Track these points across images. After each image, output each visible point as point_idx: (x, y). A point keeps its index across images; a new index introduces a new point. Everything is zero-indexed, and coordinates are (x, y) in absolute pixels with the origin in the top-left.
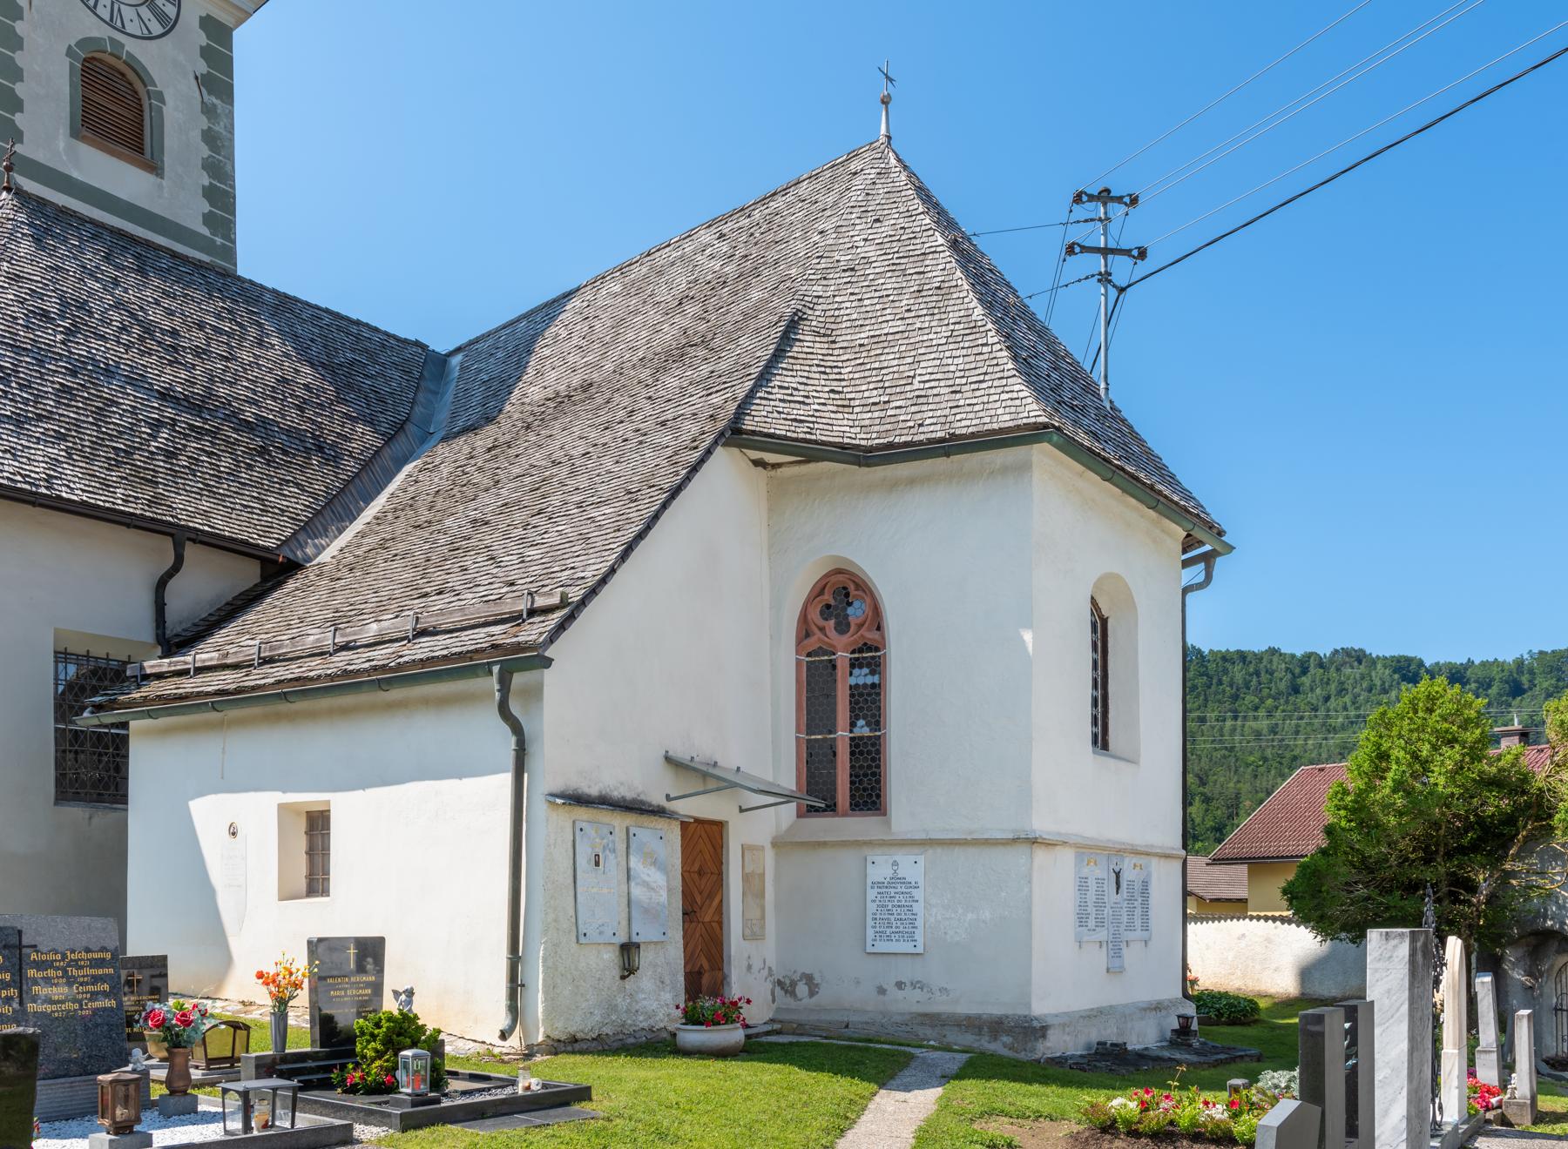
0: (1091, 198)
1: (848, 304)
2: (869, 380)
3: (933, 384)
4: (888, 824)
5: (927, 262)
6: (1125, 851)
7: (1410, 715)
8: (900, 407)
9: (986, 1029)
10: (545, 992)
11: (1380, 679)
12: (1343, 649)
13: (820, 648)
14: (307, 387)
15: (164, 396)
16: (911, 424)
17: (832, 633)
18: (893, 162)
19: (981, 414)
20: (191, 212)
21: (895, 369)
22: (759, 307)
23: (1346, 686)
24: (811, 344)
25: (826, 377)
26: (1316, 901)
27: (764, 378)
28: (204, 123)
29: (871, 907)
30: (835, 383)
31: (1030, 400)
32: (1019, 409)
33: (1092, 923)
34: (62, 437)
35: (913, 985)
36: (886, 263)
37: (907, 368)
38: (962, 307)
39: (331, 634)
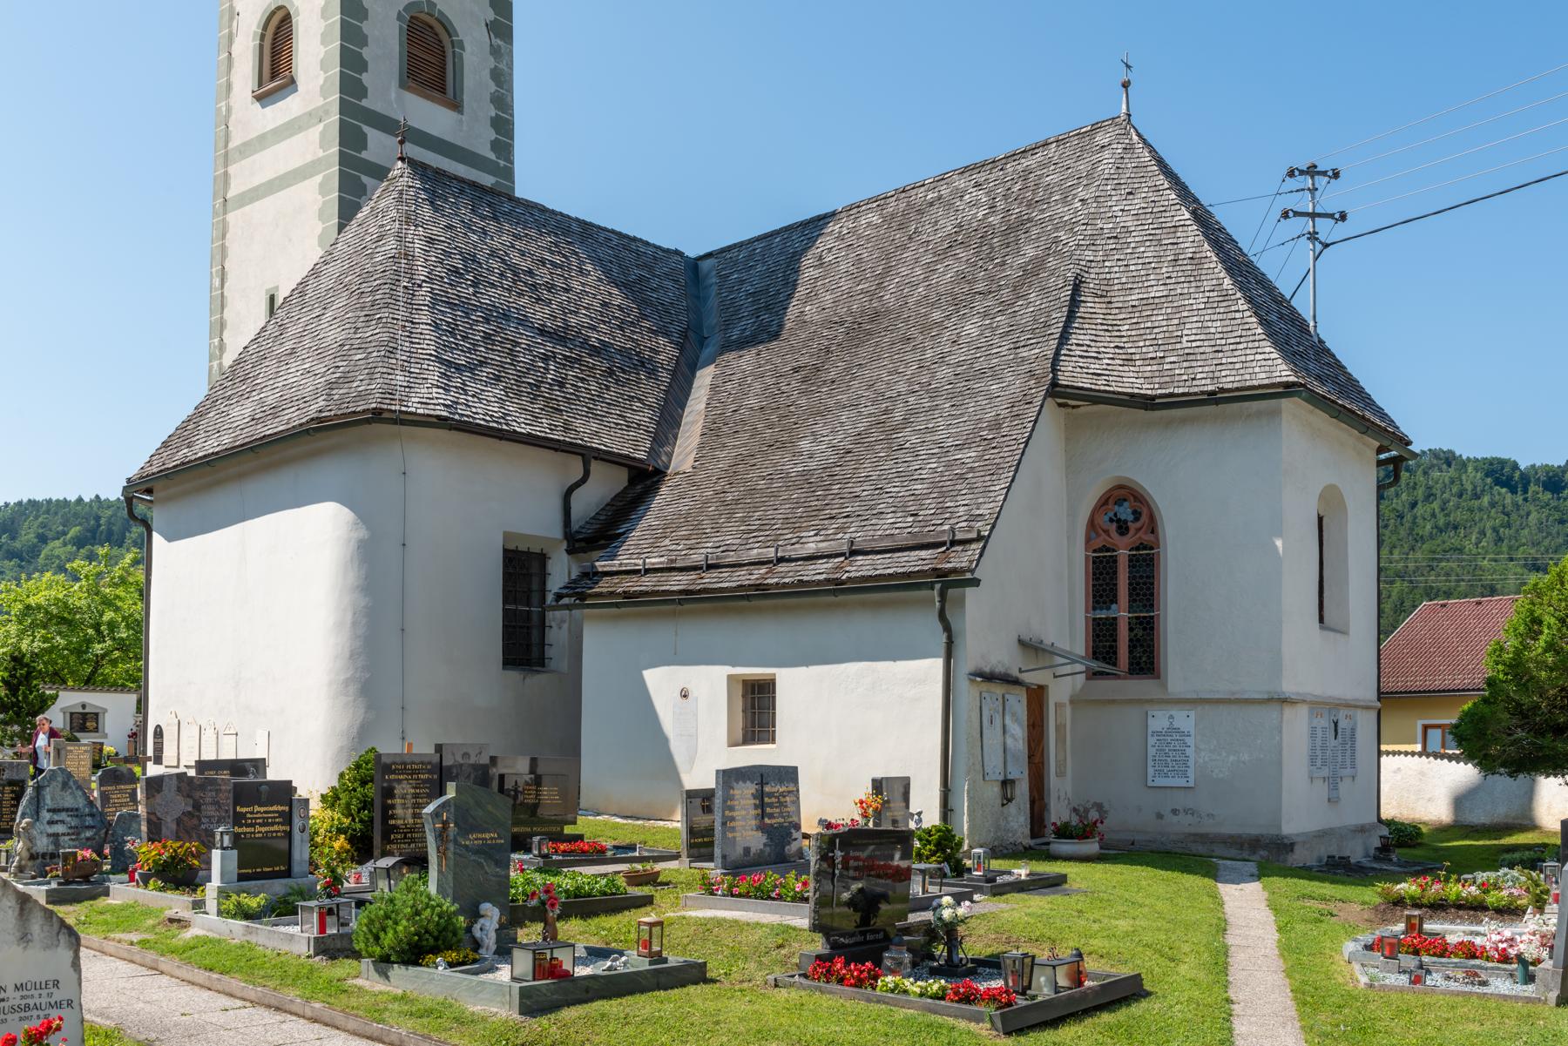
0: (1302, 172)
1: (1116, 269)
2: (1145, 337)
3: (1198, 343)
4: (1164, 686)
5: (1179, 234)
6: (1338, 705)
7: (1558, 586)
8: (1174, 362)
9: (1246, 845)
10: (969, 815)
11: (1472, 483)
12: (1430, 450)
13: (1104, 546)
14: (620, 308)
15: (542, 332)
16: (1185, 377)
17: (1114, 534)
18: (1135, 138)
19: (1242, 371)
20: (481, 141)
21: (1165, 329)
22: (1038, 264)
23: (1434, 491)
24: (1092, 305)
25: (1109, 334)
26: (1482, 743)
27: (1064, 338)
28: (491, 62)
29: (1151, 751)
30: (1117, 339)
31: (1280, 361)
32: (1273, 369)
33: (1319, 763)
34: (498, 378)
35: (1186, 812)
36: (1144, 233)
37: (1174, 328)
38: (1213, 276)
39: (773, 549)
